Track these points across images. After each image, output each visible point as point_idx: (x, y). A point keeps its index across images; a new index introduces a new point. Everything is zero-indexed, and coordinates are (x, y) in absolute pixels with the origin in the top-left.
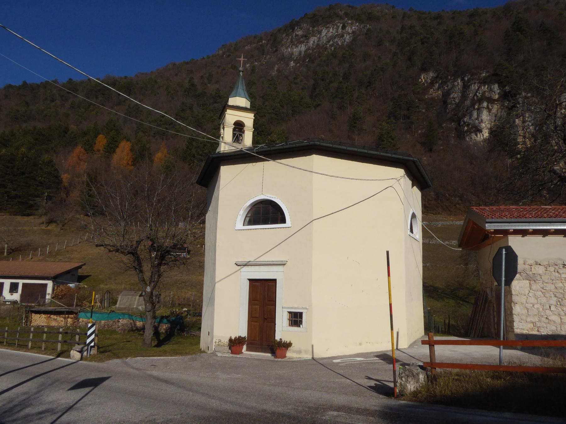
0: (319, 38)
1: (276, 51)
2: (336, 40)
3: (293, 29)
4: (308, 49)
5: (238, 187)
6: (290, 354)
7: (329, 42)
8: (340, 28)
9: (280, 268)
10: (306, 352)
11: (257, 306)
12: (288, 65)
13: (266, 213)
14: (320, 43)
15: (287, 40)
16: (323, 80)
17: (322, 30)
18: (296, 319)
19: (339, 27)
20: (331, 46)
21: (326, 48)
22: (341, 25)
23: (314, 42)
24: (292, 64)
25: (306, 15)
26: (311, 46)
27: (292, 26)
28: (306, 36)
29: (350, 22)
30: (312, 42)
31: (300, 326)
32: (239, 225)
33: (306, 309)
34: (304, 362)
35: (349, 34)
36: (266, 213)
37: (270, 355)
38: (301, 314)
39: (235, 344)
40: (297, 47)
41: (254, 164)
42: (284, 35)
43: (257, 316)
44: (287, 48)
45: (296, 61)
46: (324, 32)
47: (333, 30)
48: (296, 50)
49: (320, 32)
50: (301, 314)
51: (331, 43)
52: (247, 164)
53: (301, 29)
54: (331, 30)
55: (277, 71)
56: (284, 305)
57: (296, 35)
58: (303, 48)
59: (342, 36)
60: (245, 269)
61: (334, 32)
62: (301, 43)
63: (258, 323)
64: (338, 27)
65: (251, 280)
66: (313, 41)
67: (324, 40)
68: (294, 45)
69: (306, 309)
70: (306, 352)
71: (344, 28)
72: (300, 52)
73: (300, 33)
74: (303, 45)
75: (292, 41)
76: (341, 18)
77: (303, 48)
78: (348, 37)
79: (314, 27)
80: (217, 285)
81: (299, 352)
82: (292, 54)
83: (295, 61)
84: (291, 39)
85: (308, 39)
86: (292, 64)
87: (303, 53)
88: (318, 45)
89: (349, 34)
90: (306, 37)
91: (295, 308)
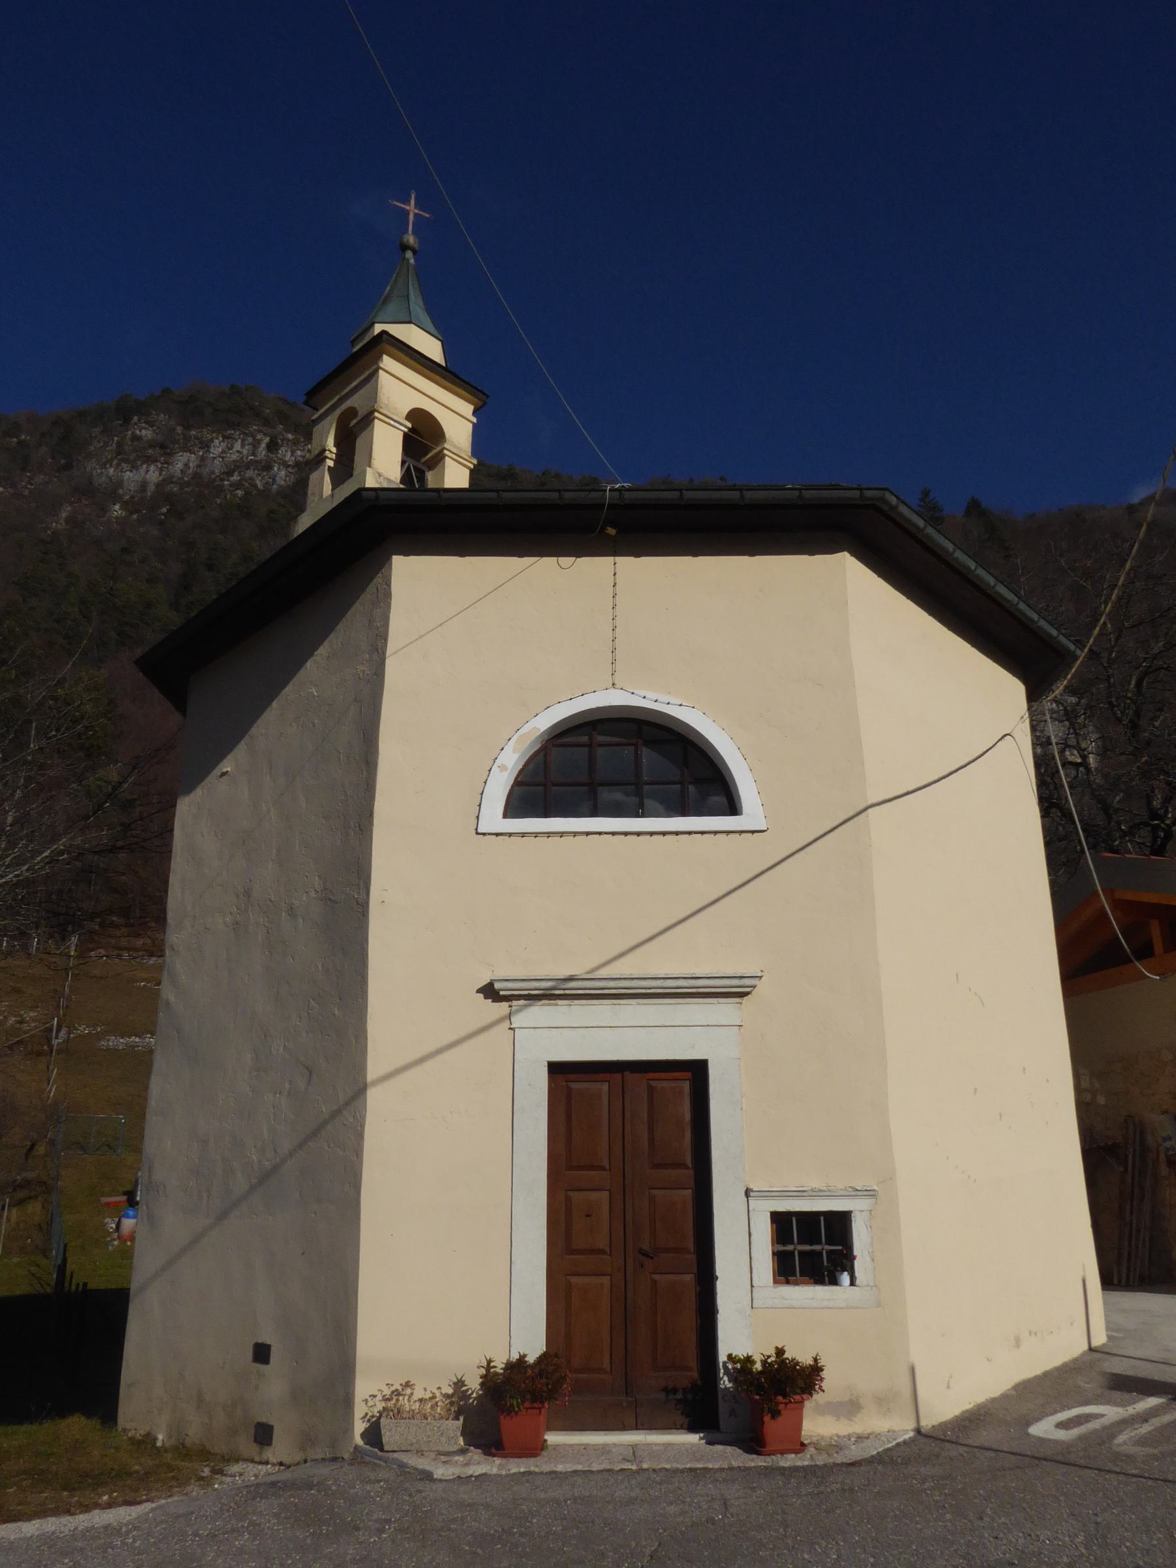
0: (203, 459)
1: (68, 467)
2: (249, 473)
3: (127, 421)
4: (169, 480)
5: (475, 653)
6: (817, 1423)
7: (230, 473)
8: (263, 445)
9: (724, 1011)
10: (884, 1402)
11: (594, 1196)
12: (104, 510)
13: (625, 763)
14: (205, 471)
15: (106, 444)
16: (210, 567)
17: (212, 440)
18: (814, 1247)
19: (259, 442)
20: (237, 485)
21: (221, 489)
22: (267, 439)
23: (186, 465)
24: (117, 510)
25: (166, 392)
26: (178, 473)
27: (126, 411)
28: (163, 446)
29: (290, 436)
30: (180, 465)
31: (834, 1282)
32: (493, 816)
33: (871, 1194)
34: (892, 1460)
35: (285, 465)
36: (625, 763)
37: (694, 1438)
38: (839, 1223)
39: (502, 1408)
40: (134, 468)
41: (566, 561)
42: (96, 431)
43: (603, 1244)
44: (104, 466)
45: (131, 506)
46: (218, 447)
47: (243, 446)
48: (131, 478)
49: (206, 446)
50: (839, 1223)
51: (235, 478)
52: (528, 560)
53: (151, 424)
54: (237, 446)
55: (67, 520)
56: (752, 1177)
57: (136, 438)
58: (153, 475)
59: (268, 467)
60: (538, 1013)
61: (245, 452)
62: (150, 460)
63: (606, 1280)
64: (256, 444)
65: (557, 1070)
66: (183, 462)
67: (217, 467)
68: (126, 461)
69: (871, 1194)
70: (884, 1402)
71: (273, 447)
72: (144, 486)
73: (147, 433)
74: (152, 468)
75: (120, 451)
76: (267, 422)
77: (153, 475)
78: (283, 473)
79: (188, 427)
80: (375, 1098)
81: (851, 1407)
82: (120, 483)
83: (125, 505)
84: (119, 444)
85: (171, 454)
86: (117, 510)
87: (151, 488)
88: (196, 476)
89: (285, 465)
90: (165, 448)
91: (817, 1194)
